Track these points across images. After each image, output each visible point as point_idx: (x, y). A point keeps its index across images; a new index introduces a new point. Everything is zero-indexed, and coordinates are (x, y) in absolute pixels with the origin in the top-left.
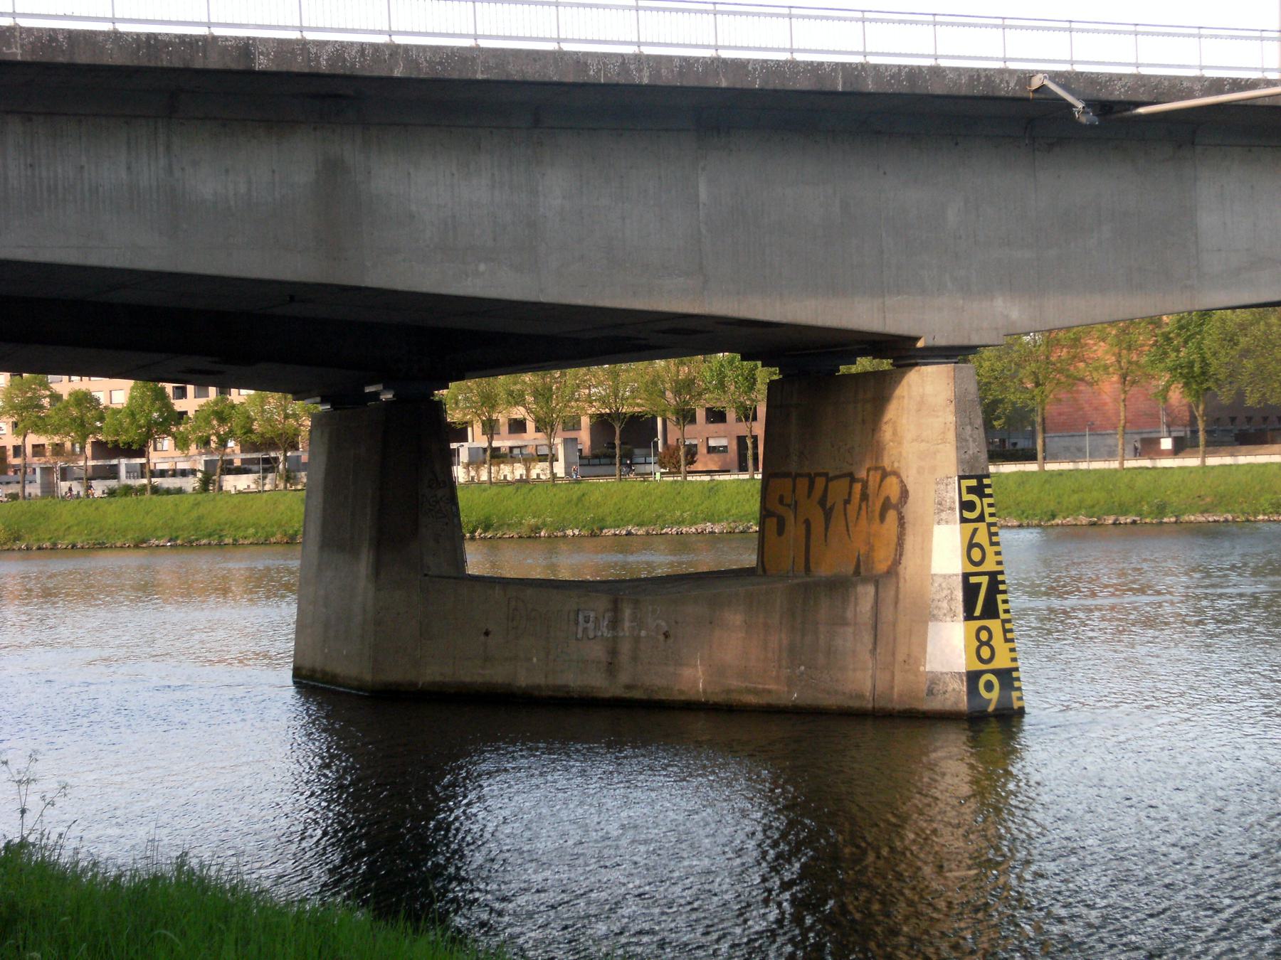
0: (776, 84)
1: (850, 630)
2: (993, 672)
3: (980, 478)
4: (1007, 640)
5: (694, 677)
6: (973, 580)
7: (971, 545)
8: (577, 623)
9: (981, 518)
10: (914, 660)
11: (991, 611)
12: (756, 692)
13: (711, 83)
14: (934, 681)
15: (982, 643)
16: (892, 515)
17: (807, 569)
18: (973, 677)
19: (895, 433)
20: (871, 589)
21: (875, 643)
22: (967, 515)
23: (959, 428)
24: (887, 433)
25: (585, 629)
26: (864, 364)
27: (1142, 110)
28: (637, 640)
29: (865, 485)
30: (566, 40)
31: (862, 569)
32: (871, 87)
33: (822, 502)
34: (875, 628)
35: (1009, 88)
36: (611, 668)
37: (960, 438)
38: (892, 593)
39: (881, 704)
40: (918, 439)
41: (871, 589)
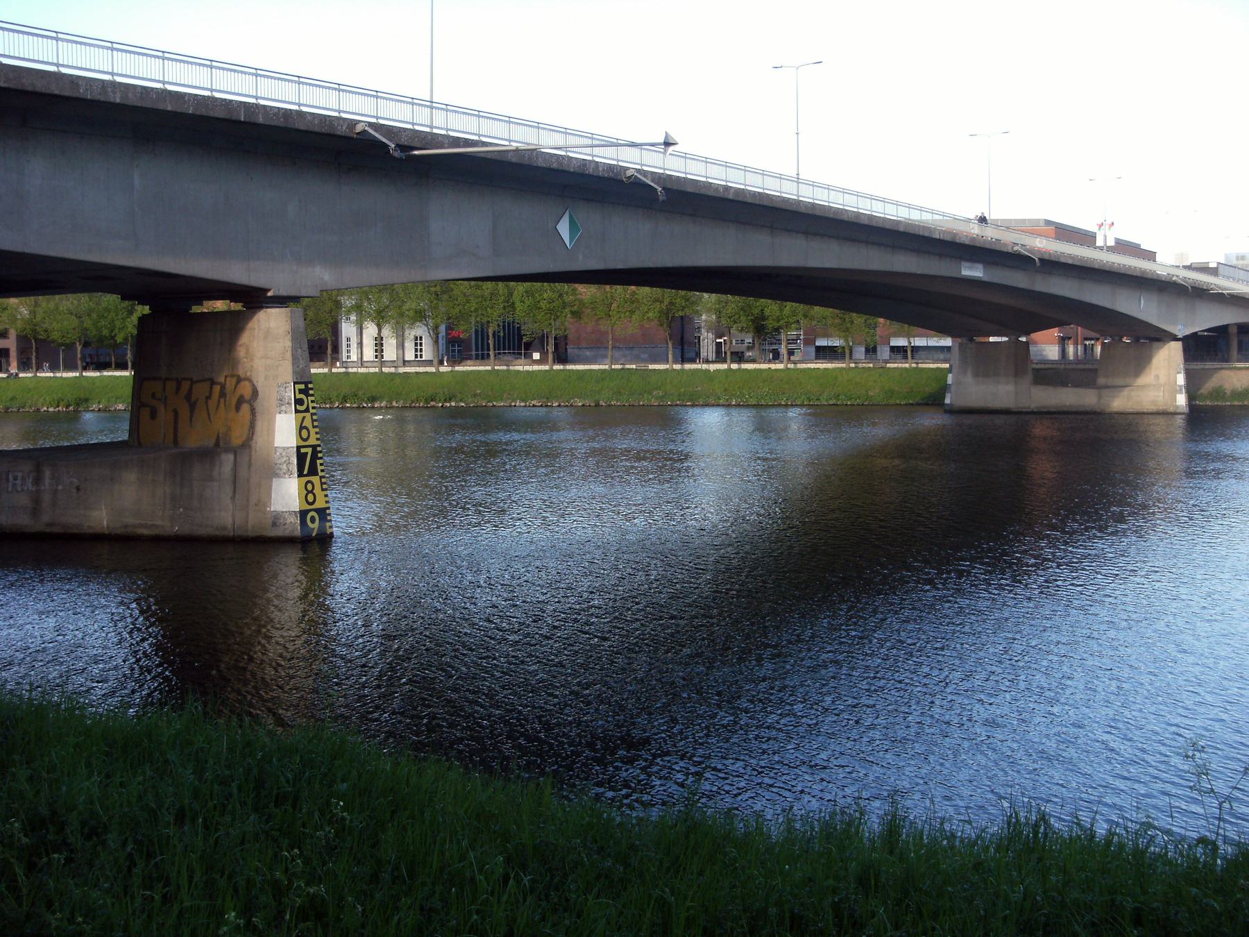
0: (203, 112)
1: (216, 484)
2: (315, 510)
3: (306, 384)
4: (323, 490)
5: (100, 517)
6: (303, 450)
7: (301, 428)
8: (8, 480)
9: (307, 410)
10: (263, 503)
11: (313, 471)
12: (146, 526)
13: (161, 106)
14: (276, 519)
15: (308, 491)
16: (245, 407)
17: (176, 442)
18: (303, 514)
19: (247, 352)
20: (231, 457)
21: (235, 492)
22: (299, 408)
23: (294, 350)
24: (241, 352)
25: (14, 485)
26: (220, 305)
27: (416, 152)
28: (55, 492)
29: (223, 387)
30: (63, 66)
31: (221, 444)
32: (261, 120)
33: (188, 397)
34: (235, 483)
35: (342, 130)
36: (35, 512)
37: (294, 358)
38: (247, 459)
39: (239, 533)
40: (266, 357)
41: (231, 457)
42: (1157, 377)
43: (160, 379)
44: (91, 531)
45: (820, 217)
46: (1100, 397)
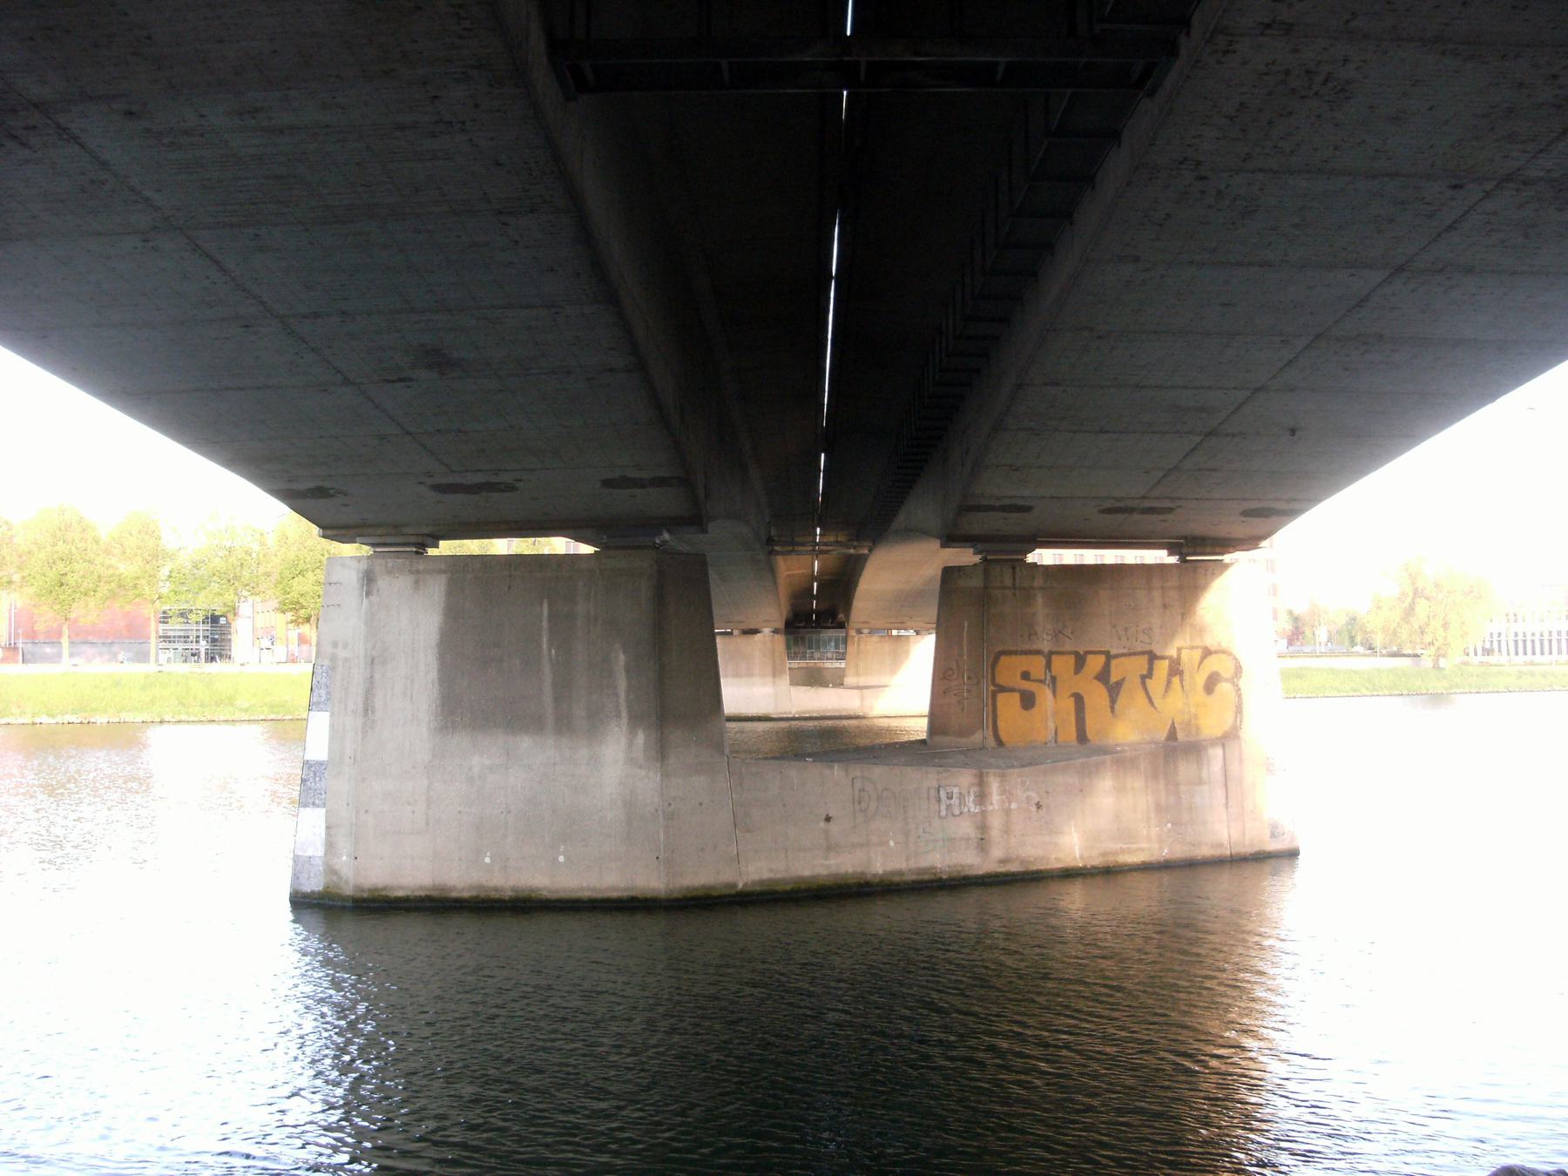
1: (1206, 788)
8: (939, 800)
16: (1224, 687)
25: (949, 807)
28: (1008, 812)
33: (1103, 676)
36: (983, 844)
43: (1038, 652)
44: (1060, 865)
46: (862, 699)
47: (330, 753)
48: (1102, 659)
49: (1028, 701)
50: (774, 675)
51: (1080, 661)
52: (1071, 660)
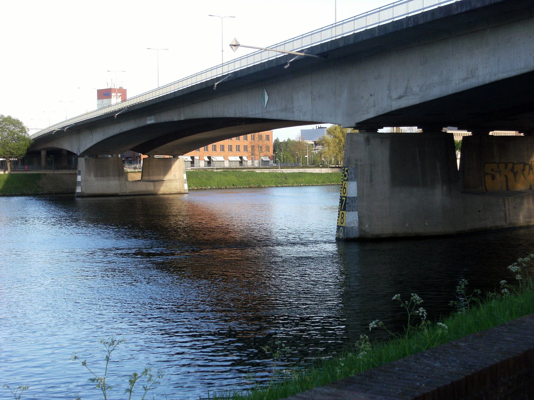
33: (512, 170)
42: (175, 175)
43: (495, 163)
45: (167, 100)
46: (155, 186)
47: (358, 194)
48: (512, 164)
49: (493, 178)
50: (119, 176)
51: (506, 165)
52: (504, 165)
